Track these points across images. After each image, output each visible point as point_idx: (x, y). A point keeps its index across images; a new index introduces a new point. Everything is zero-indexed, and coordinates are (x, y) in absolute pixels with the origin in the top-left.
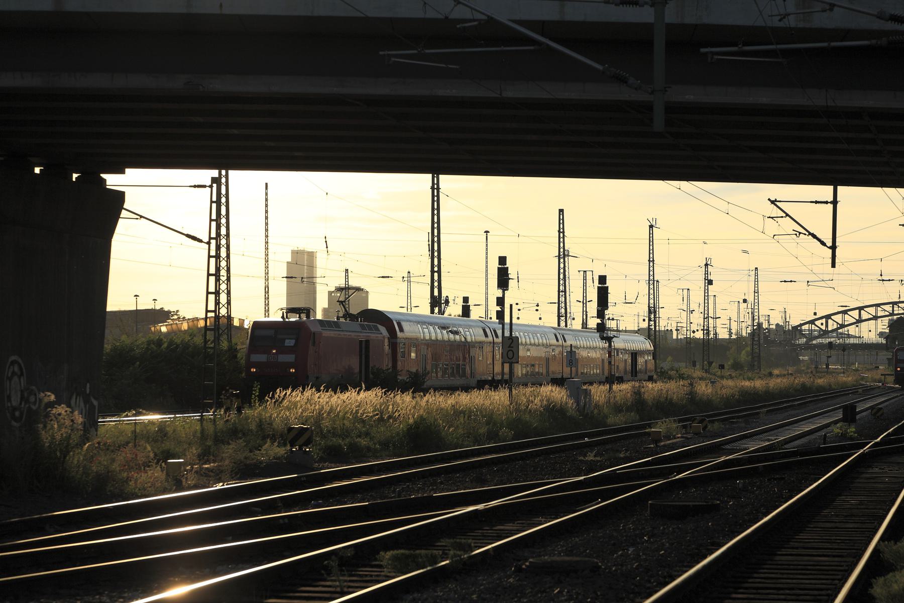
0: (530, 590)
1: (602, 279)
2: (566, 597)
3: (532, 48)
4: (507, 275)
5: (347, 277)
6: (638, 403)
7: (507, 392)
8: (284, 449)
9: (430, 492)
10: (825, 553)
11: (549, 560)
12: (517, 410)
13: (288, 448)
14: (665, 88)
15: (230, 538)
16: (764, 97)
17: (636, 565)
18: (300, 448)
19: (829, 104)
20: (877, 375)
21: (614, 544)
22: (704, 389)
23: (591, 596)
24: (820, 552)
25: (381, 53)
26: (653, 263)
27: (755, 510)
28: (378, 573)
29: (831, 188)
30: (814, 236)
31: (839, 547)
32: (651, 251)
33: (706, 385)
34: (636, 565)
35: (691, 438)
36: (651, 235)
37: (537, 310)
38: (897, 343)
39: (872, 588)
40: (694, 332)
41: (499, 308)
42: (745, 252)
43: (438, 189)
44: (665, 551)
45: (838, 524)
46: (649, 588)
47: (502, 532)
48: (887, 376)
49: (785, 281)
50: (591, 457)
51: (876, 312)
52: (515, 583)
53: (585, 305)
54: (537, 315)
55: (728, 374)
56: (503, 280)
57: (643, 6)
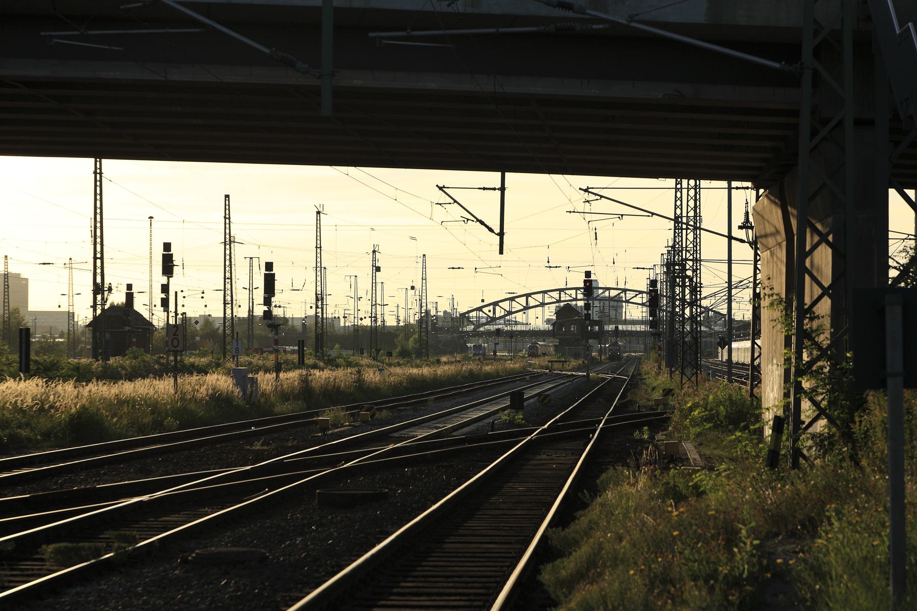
0: (196, 582)
1: (269, 266)
2: (233, 589)
3: (197, 30)
5: (6, 264)
6: (306, 392)
7: (172, 380)
10: (493, 541)
12: (183, 399)
16: (432, 82)
22: (372, 376)
24: (488, 539)
25: (43, 34)
26: (321, 250)
29: (498, 175)
30: (482, 223)
32: (318, 238)
33: (374, 373)
34: (304, 554)
36: (318, 221)
37: (202, 297)
39: (541, 574)
40: (361, 319)
41: (163, 296)
43: (101, 173)
48: (553, 363)
49: (453, 268)
54: (203, 302)
56: (168, 266)
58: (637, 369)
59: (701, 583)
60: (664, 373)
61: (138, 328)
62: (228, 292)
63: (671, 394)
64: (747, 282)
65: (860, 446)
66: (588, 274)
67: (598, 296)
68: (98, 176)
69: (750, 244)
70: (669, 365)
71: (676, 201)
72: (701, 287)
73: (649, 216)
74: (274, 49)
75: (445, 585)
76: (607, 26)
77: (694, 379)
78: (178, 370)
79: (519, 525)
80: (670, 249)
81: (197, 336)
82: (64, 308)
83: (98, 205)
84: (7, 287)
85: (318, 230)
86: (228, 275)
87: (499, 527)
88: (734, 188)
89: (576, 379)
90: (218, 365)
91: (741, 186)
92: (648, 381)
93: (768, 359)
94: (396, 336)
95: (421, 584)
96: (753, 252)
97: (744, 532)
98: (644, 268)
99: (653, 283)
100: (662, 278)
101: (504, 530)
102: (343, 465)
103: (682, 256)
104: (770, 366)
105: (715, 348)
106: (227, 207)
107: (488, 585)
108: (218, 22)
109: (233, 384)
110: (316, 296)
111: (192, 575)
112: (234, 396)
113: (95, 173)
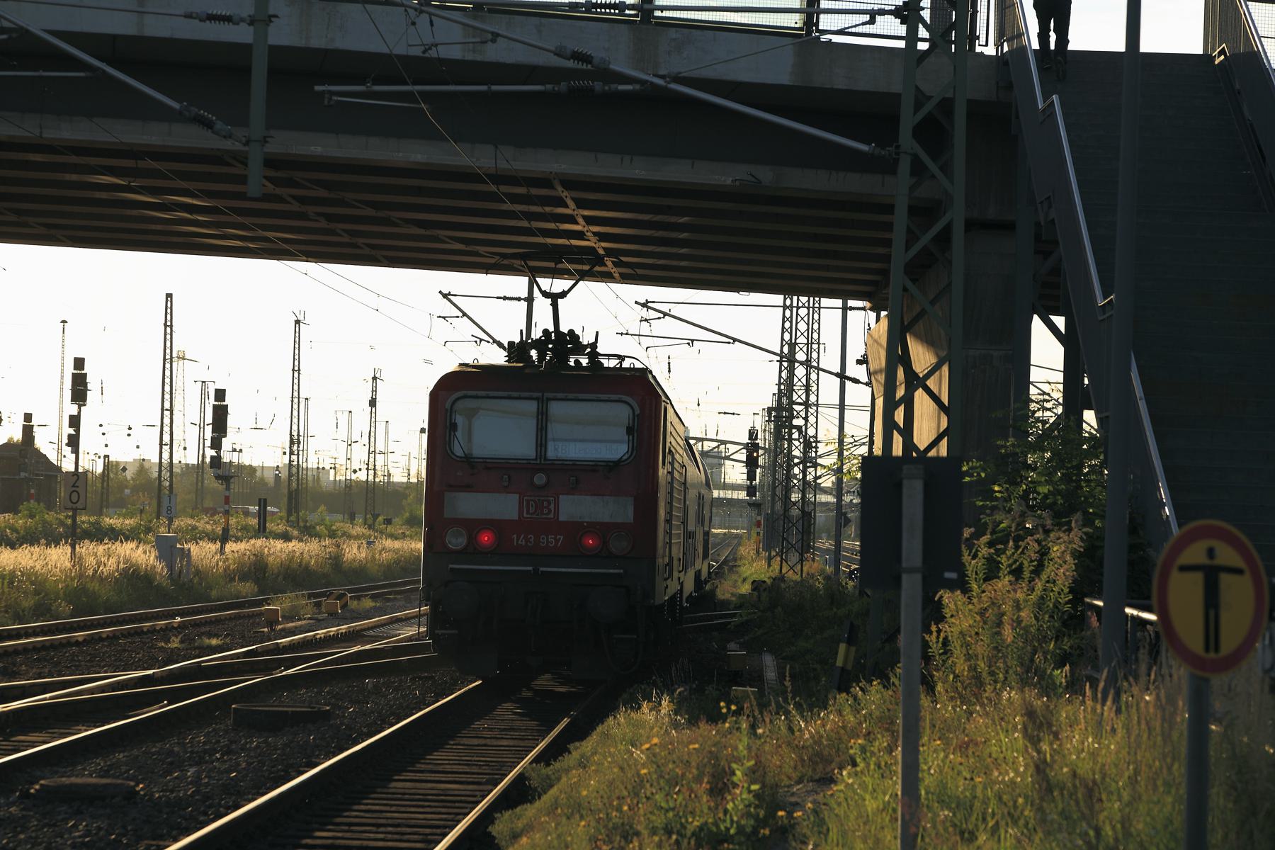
0: (35, 823)
1: (220, 394)
2: (81, 833)
3: (82, 74)
6: (257, 570)
7: (69, 549)
10: (457, 779)
11: (67, 782)
12: (81, 576)
14: (265, 137)
16: (416, 153)
21: (171, 763)
22: (354, 552)
23: (117, 831)
24: (450, 777)
26: (299, 374)
27: (380, 720)
31: (480, 771)
32: (296, 357)
33: (359, 547)
35: (323, 620)
36: (297, 334)
37: (129, 435)
40: (355, 471)
41: (72, 431)
44: (238, 772)
45: (488, 740)
47: (21, 744)
50: (175, 643)
53: (202, 430)
54: (103, 440)
55: (400, 532)
56: (79, 391)
57: (238, 24)
58: (734, 551)
61: (37, 475)
65: (937, 665)
70: (768, 548)
71: (784, 322)
73: (729, 343)
75: (372, 835)
76: (638, 87)
78: (74, 535)
79: (500, 760)
81: (127, 487)
85: (297, 346)
86: (167, 405)
87: (471, 761)
94: (405, 496)
95: (340, 835)
98: (733, 414)
99: (752, 434)
101: (477, 765)
102: (281, 672)
106: (169, 311)
108: (109, 64)
110: (291, 437)
111: (32, 813)
112: (156, 573)
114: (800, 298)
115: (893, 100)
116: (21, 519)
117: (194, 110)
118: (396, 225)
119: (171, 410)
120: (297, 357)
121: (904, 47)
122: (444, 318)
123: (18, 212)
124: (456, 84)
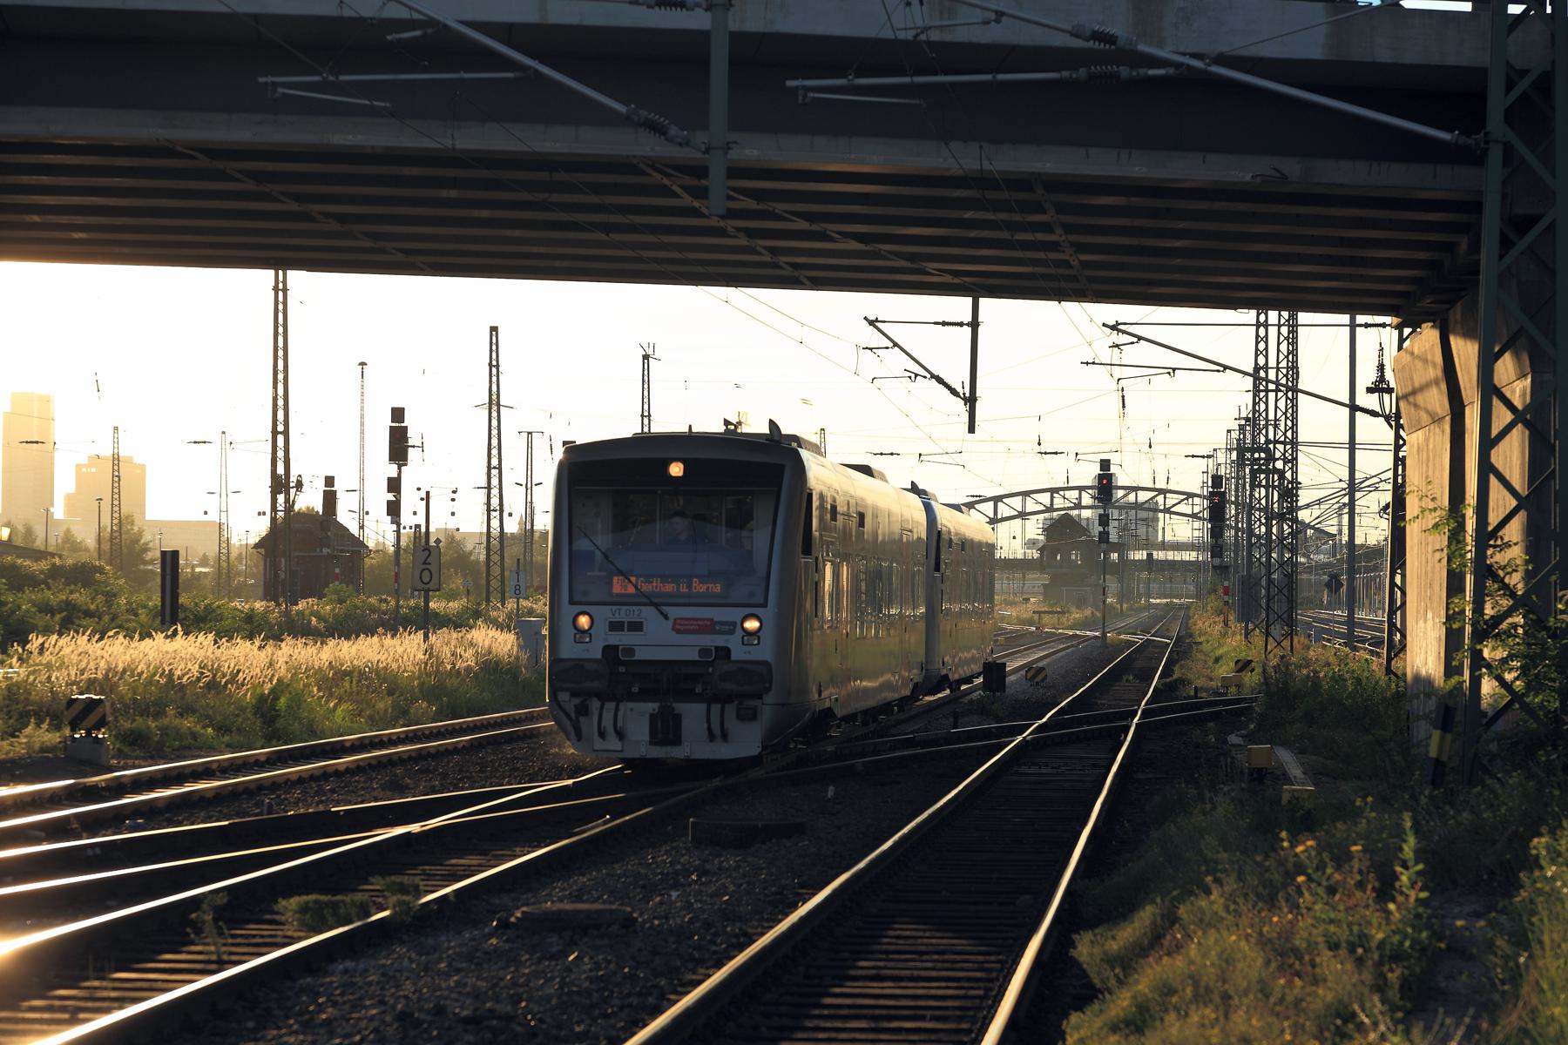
0: (527, 957)
2: (589, 966)
4: (406, 439)
5: (116, 441)
8: (58, 734)
9: (317, 805)
11: (554, 909)
13: (67, 732)
15: (10, 879)
17: (688, 917)
18: (89, 733)
19: (984, 167)
20: (1026, 611)
25: (261, 80)
26: (649, 420)
28: (273, 933)
29: (967, 302)
30: (940, 380)
34: (688, 917)
37: (453, 500)
38: (1058, 558)
39: (1075, 948)
41: (391, 497)
42: (805, 401)
43: (285, 290)
46: (715, 953)
47: (456, 868)
48: (1043, 615)
49: (882, 454)
51: (1024, 505)
52: (501, 944)
53: (529, 491)
56: (399, 447)
57: (693, 10)
58: (1186, 625)
59: (1343, 952)
60: (1234, 634)
61: (342, 551)
62: (495, 492)
63: (1249, 668)
64: (1377, 480)
66: (1105, 464)
67: (1117, 501)
68: (281, 293)
69: (1387, 418)
70: (1244, 617)
71: (1257, 343)
72: (1297, 489)
73: (1218, 371)
74: (633, 106)
75: (918, 964)
76: (1171, 71)
77: (1286, 644)
78: (426, 622)
80: (1243, 422)
82: (213, 516)
83: (281, 339)
84: (116, 478)
85: (646, 386)
86: (495, 462)
88: (1360, 325)
89: (1083, 642)
90: (477, 614)
91: (1372, 322)
92: (1206, 647)
93: (1418, 612)
95: (881, 964)
96: (1392, 433)
97: (1404, 878)
99: (1217, 480)
100: (1228, 471)
103: (1266, 436)
104: (1421, 623)
105: (1316, 592)
106: (494, 347)
107: (986, 965)
109: (519, 645)
113: (276, 289)
114: (1282, 313)
115: (1480, 74)
116: (327, 604)
117: (644, 113)
118: (832, 240)
119: (500, 468)
120: (646, 400)
121: (1470, 10)
122: (871, 349)
123: (375, 237)
124: (947, 73)
